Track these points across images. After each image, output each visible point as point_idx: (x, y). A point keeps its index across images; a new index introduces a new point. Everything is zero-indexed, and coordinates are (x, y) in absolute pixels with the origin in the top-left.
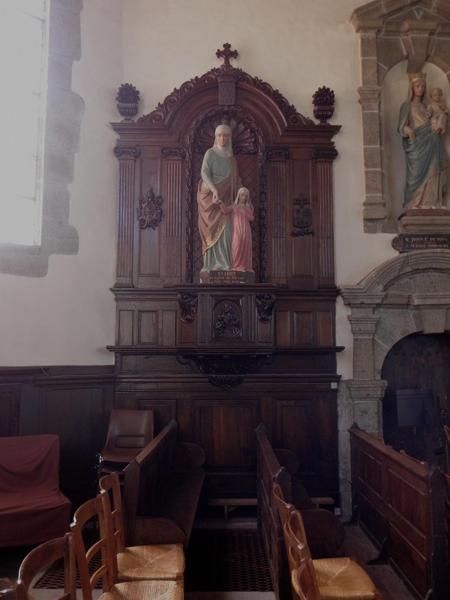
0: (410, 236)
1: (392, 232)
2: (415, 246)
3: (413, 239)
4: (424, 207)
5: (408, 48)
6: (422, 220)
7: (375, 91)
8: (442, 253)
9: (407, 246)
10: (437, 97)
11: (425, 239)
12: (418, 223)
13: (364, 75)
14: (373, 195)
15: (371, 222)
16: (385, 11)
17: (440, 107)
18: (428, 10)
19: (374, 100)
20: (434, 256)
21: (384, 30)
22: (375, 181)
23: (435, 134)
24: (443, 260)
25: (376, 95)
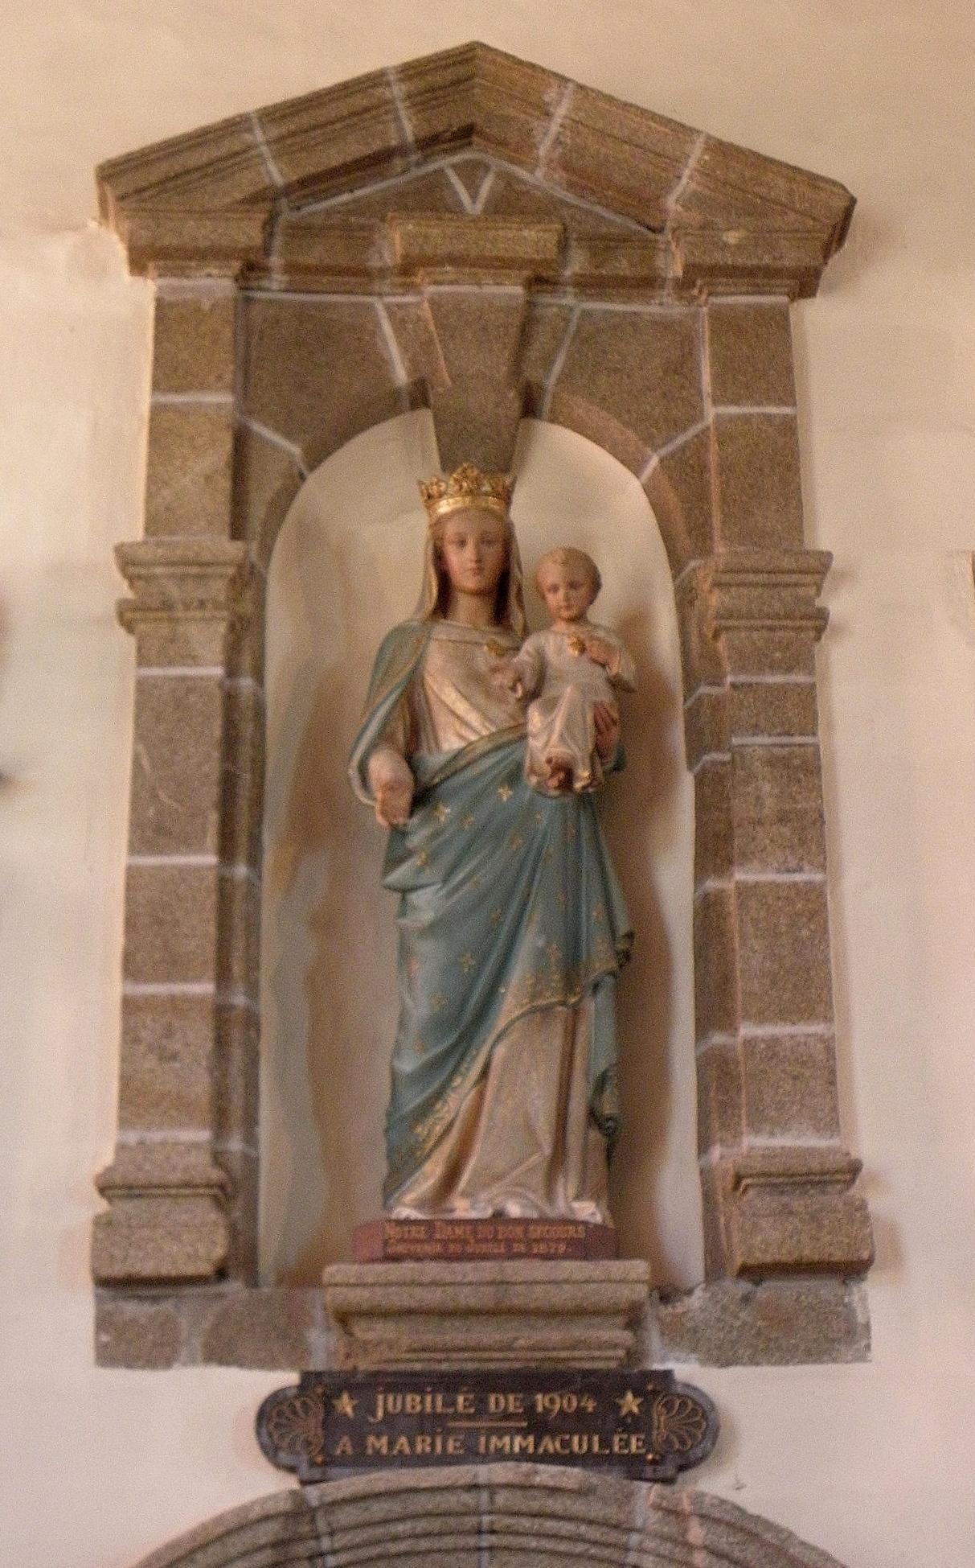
0: (364, 1386)
1: (268, 1363)
2: (391, 1444)
3: (385, 1404)
4: (462, 1208)
5: (418, 350)
6: (434, 1283)
7: (208, 564)
8: (522, 1487)
9: (345, 1445)
10: (561, 593)
11: (461, 1399)
12: (413, 1304)
13: (155, 481)
14: (156, 1136)
15: (140, 1298)
16: (276, 173)
17: (583, 649)
18: (521, 173)
19: (198, 614)
20: (477, 1512)
21: (275, 261)
22: (174, 1057)
23: (540, 791)
24: (538, 1535)
25: (218, 589)
